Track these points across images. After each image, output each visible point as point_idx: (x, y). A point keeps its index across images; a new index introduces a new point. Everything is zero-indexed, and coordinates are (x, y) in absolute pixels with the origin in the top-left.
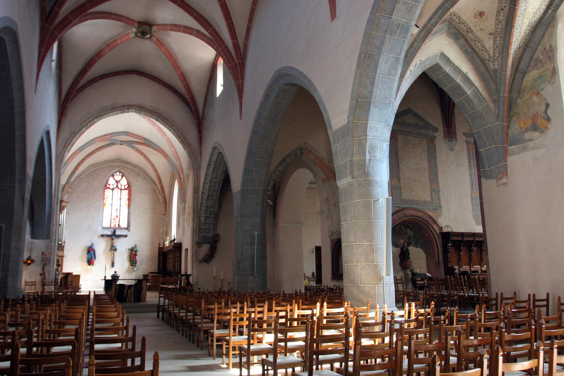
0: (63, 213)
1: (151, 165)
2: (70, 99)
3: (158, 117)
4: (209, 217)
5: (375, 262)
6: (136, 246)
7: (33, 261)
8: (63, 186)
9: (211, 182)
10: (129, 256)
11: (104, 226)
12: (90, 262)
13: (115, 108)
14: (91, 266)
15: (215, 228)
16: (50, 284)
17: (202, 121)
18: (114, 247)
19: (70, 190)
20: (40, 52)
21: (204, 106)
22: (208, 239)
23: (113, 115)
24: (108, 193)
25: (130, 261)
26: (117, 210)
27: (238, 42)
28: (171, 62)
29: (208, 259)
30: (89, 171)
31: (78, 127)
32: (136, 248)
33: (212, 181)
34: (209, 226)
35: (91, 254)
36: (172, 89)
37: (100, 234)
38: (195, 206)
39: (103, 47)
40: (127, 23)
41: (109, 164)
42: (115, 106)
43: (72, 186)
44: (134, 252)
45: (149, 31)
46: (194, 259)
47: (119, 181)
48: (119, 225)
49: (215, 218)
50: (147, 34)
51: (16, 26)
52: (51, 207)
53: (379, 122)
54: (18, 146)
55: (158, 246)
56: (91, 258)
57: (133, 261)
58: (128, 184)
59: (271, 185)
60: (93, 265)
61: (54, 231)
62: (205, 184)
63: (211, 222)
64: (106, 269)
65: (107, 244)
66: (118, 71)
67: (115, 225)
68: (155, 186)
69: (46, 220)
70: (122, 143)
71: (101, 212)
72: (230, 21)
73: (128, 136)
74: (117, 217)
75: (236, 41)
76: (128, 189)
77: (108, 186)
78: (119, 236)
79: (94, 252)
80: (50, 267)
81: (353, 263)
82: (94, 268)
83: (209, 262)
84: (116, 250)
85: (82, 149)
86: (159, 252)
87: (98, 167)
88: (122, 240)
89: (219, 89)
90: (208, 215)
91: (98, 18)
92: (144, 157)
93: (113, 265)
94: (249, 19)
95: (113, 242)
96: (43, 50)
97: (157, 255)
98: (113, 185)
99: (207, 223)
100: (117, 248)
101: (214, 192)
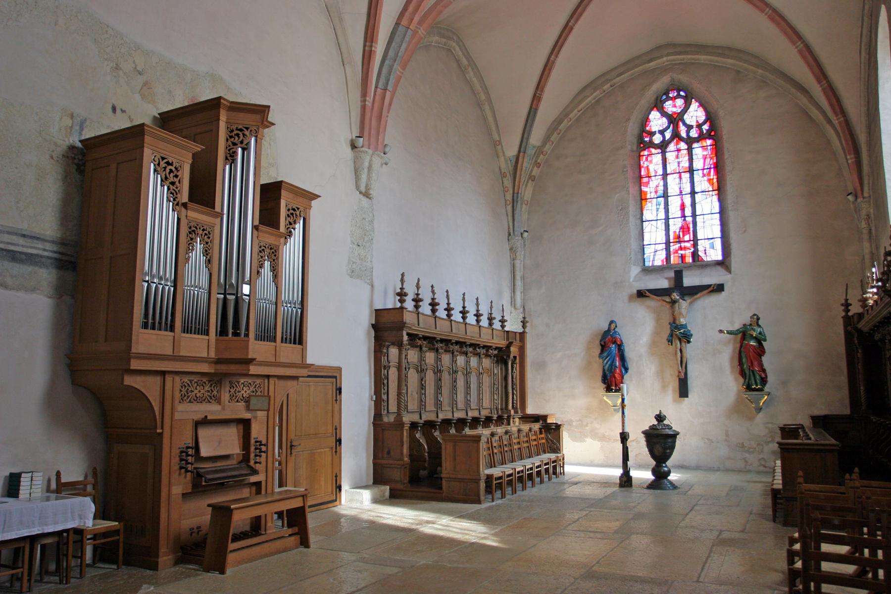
1: (771, 19)
8: (514, 160)
10: (737, 355)
19: (536, 172)
25: (742, 373)
41: (640, 68)
44: (753, 343)
48: (695, 255)
58: (709, 118)
65: (658, 320)
67: (683, 257)
68: (803, 100)
71: (633, 221)
74: (685, 229)
79: (620, 347)
84: (686, 337)
86: (848, 335)
88: (706, 302)
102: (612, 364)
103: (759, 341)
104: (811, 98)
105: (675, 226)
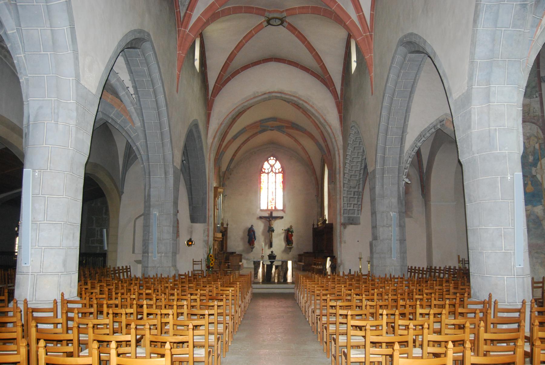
4: (353, 198)
5: (503, 249)
6: (291, 227)
15: (360, 208)
24: (264, 177)
26: (273, 193)
27: (363, 14)
37: (259, 216)
42: (257, 95)
47: (274, 165)
48: (275, 207)
53: (505, 84)
58: (282, 167)
59: (408, 162)
63: (356, 202)
65: (265, 226)
67: (272, 207)
74: (273, 199)
75: (361, 13)
77: (263, 170)
81: (478, 250)
84: (273, 231)
93: (271, 246)
95: (271, 224)
98: (268, 169)
100: (275, 228)
101: (356, 172)
103: (292, 232)
105: (270, 199)
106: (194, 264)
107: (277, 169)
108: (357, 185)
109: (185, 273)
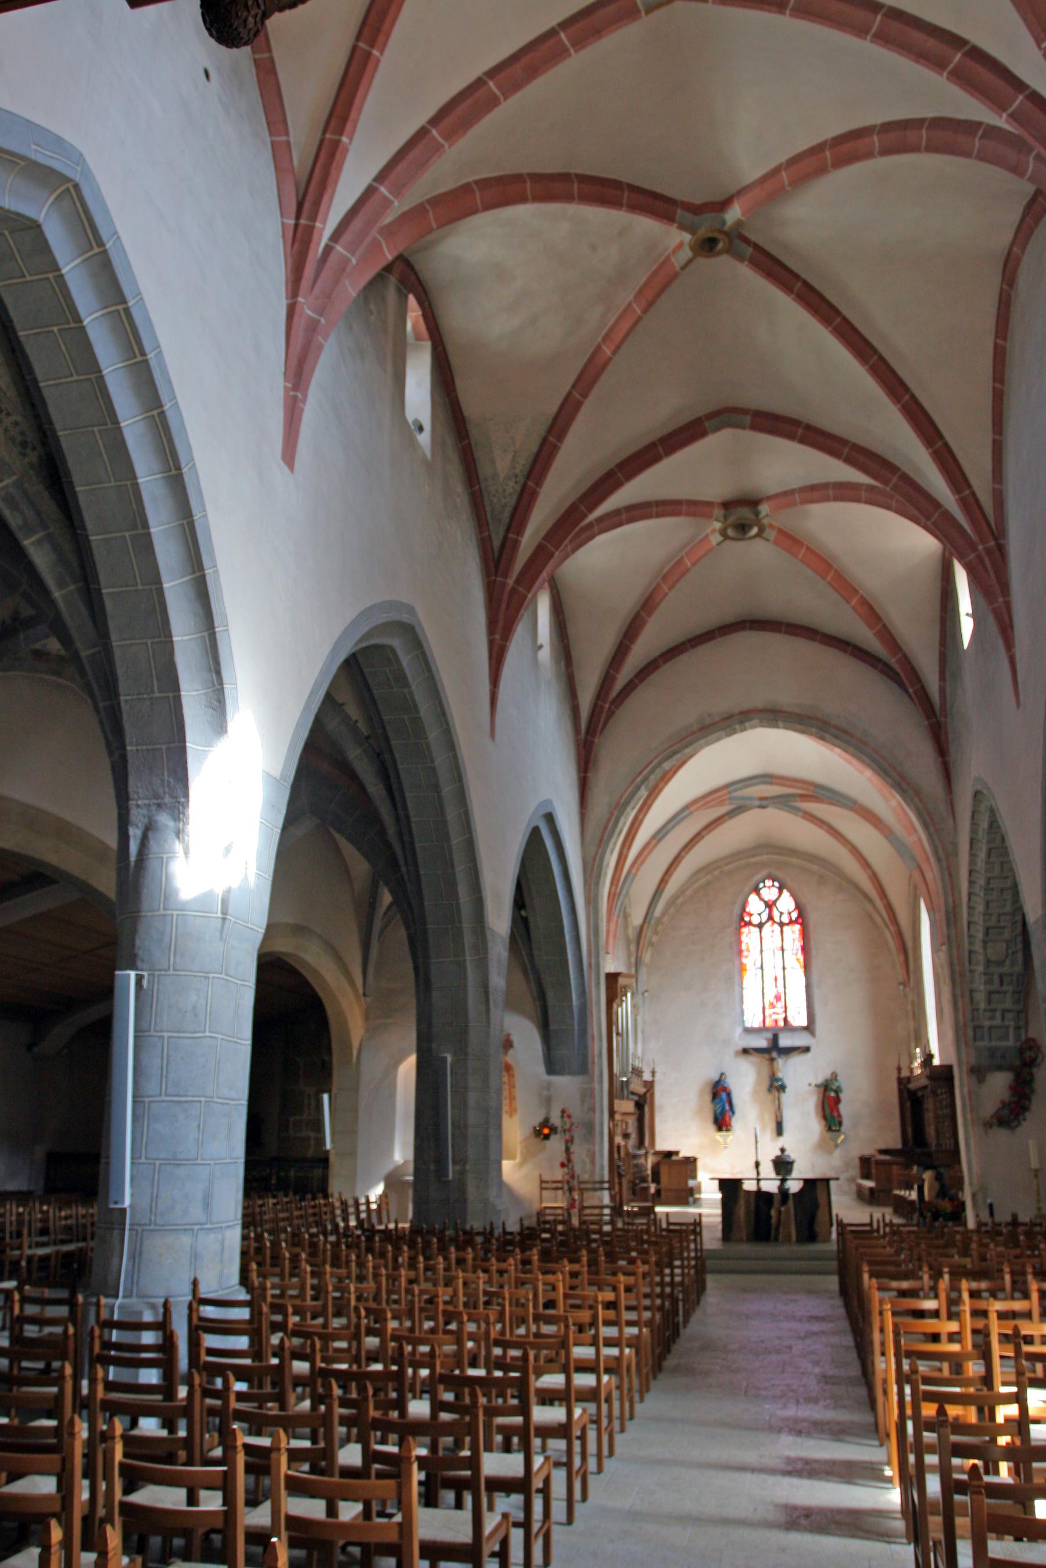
0: (624, 1004)
2: (601, 725)
3: (821, 729)
4: (998, 992)
6: (834, 1076)
7: (553, 1130)
9: (988, 889)
11: (748, 1025)
12: (722, 1123)
13: (709, 725)
14: (723, 1133)
15: (1022, 1023)
16: (598, 1186)
17: (943, 720)
18: (778, 1080)
19: (655, 939)
20: (491, 643)
21: (942, 678)
22: (1003, 1057)
23: (708, 744)
24: (749, 937)
25: (825, 1117)
26: (776, 979)
27: (973, 494)
28: (829, 578)
29: (1012, 1117)
30: (696, 886)
31: (626, 790)
32: (836, 1080)
33: (991, 886)
34: (1003, 1019)
35: (721, 1100)
36: (850, 648)
38: (956, 961)
39: (654, 585)
40: (694, 515)
41: (743, 862)
42: (708, 721)
43: (660, 927)
44: (833, 1094)
45: (751, 516)
46: (969, 1116)
47: (775, 902)
48: (785, 1020)
49: (1020, 992)
50: (750, 527)
51: (411, 610)
52: (583, 993)
54: (460, 870)
55: (895, 1075)
56: (723, 1112)
57: (833, 1117)
58: (798, 907)
60: (728, 1130)
61: (596, 1052)
62: (973, 897)
63: (1008, 1005)
64: (756, 1142)
65: (759, 1073)
66: (705, 630)
67: (776, 1021)
68: (869, 907)
69: (576, 1028)
70: (764, 803)
71: (737, 988)
72: (940, 444)
73: (771, 783)
74: (778, 998)
76: (800, 921)
77: (747, 919)
78: (788, 1051)
79: (729, 1095)
80: (594, 1144)
82: (731, 1137)
83: (1016, 1126)
84: (782, 1088)
85: (661, 834)
86: (901, 1092)
87: (717, 872)
89: (967, 627)
90: (996, 986)
91: (620, 524)
92: (827, 832)
93: (779, 1130)
94: (994, 424)
96: (497, 637)
97: (895, 1099)
98: (760, 914)
99: (994, 1010)
101: (1003, 918)
102: (724, 1107)
103: (837, 1091)
104: (875, 907)
105: (770, 997)
106: (542, 1189)
107: (785, 911)
108: (1007, 957)
109: (485, 1229)
